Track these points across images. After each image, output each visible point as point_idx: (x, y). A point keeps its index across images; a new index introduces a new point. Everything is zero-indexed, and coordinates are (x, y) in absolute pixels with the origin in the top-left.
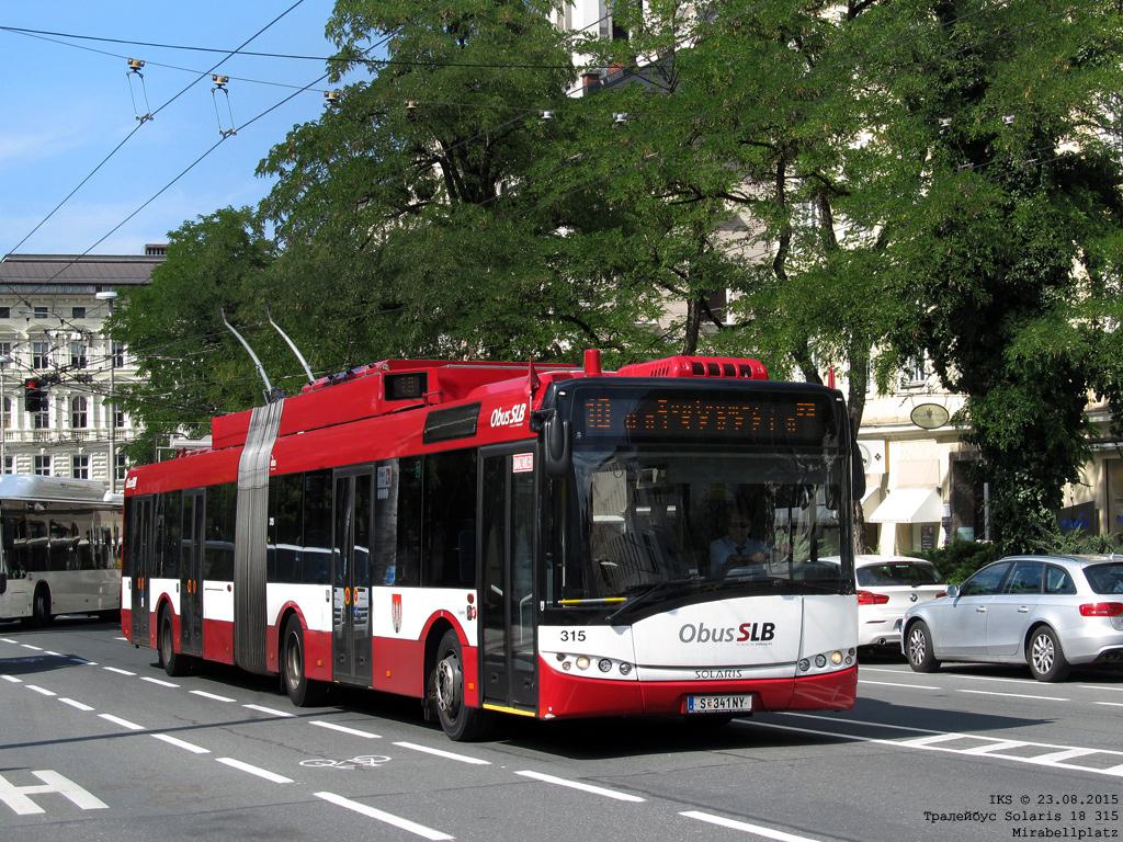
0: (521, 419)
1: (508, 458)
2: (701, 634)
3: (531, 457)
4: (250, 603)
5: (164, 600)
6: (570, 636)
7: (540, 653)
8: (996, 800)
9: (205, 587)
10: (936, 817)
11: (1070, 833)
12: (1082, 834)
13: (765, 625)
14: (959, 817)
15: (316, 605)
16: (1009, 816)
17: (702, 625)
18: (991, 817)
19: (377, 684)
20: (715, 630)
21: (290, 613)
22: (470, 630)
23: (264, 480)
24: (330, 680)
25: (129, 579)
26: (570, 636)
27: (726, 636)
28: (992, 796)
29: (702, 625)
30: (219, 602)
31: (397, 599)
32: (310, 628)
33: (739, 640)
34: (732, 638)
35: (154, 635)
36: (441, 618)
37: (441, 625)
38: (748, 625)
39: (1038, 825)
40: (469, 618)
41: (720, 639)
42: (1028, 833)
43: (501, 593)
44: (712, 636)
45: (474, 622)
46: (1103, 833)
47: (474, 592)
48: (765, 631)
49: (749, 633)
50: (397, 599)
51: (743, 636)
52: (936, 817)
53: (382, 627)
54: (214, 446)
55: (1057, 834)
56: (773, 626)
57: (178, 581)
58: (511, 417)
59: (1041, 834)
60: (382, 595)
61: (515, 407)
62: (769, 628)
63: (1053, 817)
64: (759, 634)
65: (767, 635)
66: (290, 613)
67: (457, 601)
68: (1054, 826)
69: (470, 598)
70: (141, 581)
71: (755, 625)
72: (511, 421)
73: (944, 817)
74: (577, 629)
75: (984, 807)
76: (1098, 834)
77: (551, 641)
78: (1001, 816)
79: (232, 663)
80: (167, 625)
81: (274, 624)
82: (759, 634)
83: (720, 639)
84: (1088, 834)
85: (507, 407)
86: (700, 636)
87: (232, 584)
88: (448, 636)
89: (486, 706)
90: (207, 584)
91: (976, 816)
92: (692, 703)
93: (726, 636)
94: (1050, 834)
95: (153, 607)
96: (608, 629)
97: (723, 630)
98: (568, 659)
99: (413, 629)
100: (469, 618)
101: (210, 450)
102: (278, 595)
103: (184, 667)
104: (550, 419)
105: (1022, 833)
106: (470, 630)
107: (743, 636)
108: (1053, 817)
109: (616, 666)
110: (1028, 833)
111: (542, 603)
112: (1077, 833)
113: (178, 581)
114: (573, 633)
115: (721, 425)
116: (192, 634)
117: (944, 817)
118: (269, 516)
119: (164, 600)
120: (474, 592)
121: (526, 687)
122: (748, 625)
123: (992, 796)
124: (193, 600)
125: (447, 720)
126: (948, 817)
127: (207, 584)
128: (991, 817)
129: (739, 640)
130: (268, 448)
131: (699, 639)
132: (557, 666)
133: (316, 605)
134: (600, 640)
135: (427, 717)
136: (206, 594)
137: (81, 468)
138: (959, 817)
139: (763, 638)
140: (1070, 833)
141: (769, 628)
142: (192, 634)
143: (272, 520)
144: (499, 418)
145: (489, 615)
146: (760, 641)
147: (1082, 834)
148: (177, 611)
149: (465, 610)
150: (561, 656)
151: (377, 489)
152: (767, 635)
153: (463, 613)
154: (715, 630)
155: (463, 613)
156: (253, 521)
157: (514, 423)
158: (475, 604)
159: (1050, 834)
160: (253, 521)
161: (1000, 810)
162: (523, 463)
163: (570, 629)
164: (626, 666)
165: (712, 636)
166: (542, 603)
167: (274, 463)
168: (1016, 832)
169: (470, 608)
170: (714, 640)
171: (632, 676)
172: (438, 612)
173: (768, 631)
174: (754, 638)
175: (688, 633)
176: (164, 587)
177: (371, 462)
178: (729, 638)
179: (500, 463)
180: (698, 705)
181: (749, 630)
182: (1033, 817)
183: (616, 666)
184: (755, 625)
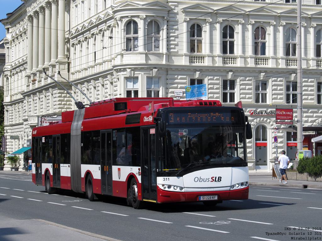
0: (152, 120)
1: (149, 130)
2: (200, 180)
3: (155, 130)
4: (76, 171)
5: (47, 170)
6: (166, 179)
7: (158, 185)
8: (286, 229)
9: (61, 166)
10: (269, 234)
11: (307, 238)
12: (311, 239)
13: (219, 177)
14: (276, 234)
15: (96, 171)
16: (290, 234)
17: (200, 177)
18: (285, 234)
19: (114, 195)
20: (204, 179)
21: (88, 173)
22: (139, 178)
23: (79, 133)
24: (101, 194)
25: (35, 164)
26: (166, 179)
27: (207, 180)
28: (285, 228)
29: (200, 177)
30: (65, 170)
31: (119, 169)
32: (94, 178)
33: (211, 181)
34: (209, 181)
35: (44, 182)
36: (131, 175)
37: (131, 177)
38: (214, 177)
39: (298, 236)
40: (139, 175)
41: (206, 181)
42: (296, 238)
43: (147, 168)
44: (203, 180)
45: (140, 176)
46: (317, 239)
47: (140, 167)
48: (219, 179)
49: (214, 179)
50: (119, 169)
51: (212, 180)
52: (269, 234)
53: (115, 178)
54: (63, 120)
55: (304, 239)
56: (221, 178)
57: (52, 164)
58: (149, 119)
59: (299, 239)
60: (115, 168)
61: (150, 116)
62: (220, 178)
63: (302, 234)
64: (217, 180)
65: (219, 180)
66: (88, 173)
67: (135, 170)
68: (303, 236)
69: (139, 169)
70: (106, 168)
71: (216, 177)
72: (149, 120)
73: (271, 234)
74: (168, 177)
75: (283, 231)
76: (316, 239)
77: (161, 182)
78: (288, 234)
79: (70, 189)
80: (48, 178)
81: (83, 177)
82: (217, 180)
83: (206, 181)
84: (312, 239)
85: (148, 116)
86: (200, 180)
87: (70, 165)
88: (133, 179)
89: (144, 200)
90: (61, 165)
91: (281, 234)
92: (200, 198)
93: (207, 180)
94: (302, 239)
95: (43, 173)
96: (176, 177)
97: (206, 179)
98: (165, 186)
99: (124, 179)
100: (139, 175)
101: (60, 122)
102: (85, 168)
103: (54, 191)
104: (160, 120)
105: (294, 238)
106: (139, 178)
107: (212, 180)
108: (302, 234)
109: (178, 188)
110: (296, 238)
111: (158, 170)
112: (309, 239)
113: (52, 164)
114: (167, 178)
115: (209, 120)
116: (57, 181)
117: (271, 234)
118: (81, 143)
119: (47, 170)
120: (140, 167)
121: (155, 194)
122: (214, 177)
123: (285, 228)
124: (57, 170)
125: (133, 204)
126: (272, 234)
127: (61, 165)
128: (285, 234)
129: (211, 181)
130: (80, 123)
131: (200, 181)
132: (162, 188)
133: (96, 171)
134: (173, 180)
135: (128, 204)
136: (61, 168)
137: (228, 91)
138: (276, 234)
139: (218, 181)
140: (307, 238)
141: (220, 178)
142: (57, 181)
143: (82, 144)
144: (146, 119)
145: (143, 173)
146: (217, 182)
147: (311, 239)
148: (52, 174)
149: (138, 173)
150: (163, 185)
151: (113, 137)
152: (219, 180)
153: (137, 174)
154: (204, 179)
155: (137, 174)
156: (76, 145)
157: (150, 121)
158: (140, 171)
159: (302, 239)
160: (76, 145)
161: (288, 232)
162: (153, 131)
163: (165, 177)
164: (181, 188)
165: (203, 180)
166: (158, 170)
167: (82, 127)
168: (292, 238)
169: (139, 172)
170: (204, 181)
171: (183, 191)
172: (130, 173)
173: (220, 179)
174: (215, 181)
175: (196, 179)
176: (47, 166)
177: (111, 129)
178: (208, 181)
179: (147, 131)
180: (202, 198)
181: (214, 179)
182: (297, 234)
183: (172, 187)
184: (216, 177)
